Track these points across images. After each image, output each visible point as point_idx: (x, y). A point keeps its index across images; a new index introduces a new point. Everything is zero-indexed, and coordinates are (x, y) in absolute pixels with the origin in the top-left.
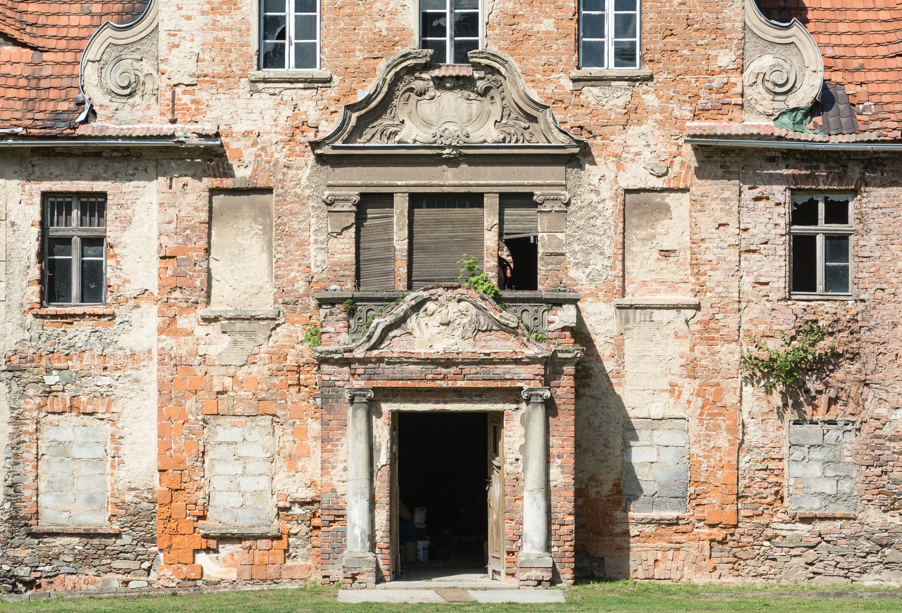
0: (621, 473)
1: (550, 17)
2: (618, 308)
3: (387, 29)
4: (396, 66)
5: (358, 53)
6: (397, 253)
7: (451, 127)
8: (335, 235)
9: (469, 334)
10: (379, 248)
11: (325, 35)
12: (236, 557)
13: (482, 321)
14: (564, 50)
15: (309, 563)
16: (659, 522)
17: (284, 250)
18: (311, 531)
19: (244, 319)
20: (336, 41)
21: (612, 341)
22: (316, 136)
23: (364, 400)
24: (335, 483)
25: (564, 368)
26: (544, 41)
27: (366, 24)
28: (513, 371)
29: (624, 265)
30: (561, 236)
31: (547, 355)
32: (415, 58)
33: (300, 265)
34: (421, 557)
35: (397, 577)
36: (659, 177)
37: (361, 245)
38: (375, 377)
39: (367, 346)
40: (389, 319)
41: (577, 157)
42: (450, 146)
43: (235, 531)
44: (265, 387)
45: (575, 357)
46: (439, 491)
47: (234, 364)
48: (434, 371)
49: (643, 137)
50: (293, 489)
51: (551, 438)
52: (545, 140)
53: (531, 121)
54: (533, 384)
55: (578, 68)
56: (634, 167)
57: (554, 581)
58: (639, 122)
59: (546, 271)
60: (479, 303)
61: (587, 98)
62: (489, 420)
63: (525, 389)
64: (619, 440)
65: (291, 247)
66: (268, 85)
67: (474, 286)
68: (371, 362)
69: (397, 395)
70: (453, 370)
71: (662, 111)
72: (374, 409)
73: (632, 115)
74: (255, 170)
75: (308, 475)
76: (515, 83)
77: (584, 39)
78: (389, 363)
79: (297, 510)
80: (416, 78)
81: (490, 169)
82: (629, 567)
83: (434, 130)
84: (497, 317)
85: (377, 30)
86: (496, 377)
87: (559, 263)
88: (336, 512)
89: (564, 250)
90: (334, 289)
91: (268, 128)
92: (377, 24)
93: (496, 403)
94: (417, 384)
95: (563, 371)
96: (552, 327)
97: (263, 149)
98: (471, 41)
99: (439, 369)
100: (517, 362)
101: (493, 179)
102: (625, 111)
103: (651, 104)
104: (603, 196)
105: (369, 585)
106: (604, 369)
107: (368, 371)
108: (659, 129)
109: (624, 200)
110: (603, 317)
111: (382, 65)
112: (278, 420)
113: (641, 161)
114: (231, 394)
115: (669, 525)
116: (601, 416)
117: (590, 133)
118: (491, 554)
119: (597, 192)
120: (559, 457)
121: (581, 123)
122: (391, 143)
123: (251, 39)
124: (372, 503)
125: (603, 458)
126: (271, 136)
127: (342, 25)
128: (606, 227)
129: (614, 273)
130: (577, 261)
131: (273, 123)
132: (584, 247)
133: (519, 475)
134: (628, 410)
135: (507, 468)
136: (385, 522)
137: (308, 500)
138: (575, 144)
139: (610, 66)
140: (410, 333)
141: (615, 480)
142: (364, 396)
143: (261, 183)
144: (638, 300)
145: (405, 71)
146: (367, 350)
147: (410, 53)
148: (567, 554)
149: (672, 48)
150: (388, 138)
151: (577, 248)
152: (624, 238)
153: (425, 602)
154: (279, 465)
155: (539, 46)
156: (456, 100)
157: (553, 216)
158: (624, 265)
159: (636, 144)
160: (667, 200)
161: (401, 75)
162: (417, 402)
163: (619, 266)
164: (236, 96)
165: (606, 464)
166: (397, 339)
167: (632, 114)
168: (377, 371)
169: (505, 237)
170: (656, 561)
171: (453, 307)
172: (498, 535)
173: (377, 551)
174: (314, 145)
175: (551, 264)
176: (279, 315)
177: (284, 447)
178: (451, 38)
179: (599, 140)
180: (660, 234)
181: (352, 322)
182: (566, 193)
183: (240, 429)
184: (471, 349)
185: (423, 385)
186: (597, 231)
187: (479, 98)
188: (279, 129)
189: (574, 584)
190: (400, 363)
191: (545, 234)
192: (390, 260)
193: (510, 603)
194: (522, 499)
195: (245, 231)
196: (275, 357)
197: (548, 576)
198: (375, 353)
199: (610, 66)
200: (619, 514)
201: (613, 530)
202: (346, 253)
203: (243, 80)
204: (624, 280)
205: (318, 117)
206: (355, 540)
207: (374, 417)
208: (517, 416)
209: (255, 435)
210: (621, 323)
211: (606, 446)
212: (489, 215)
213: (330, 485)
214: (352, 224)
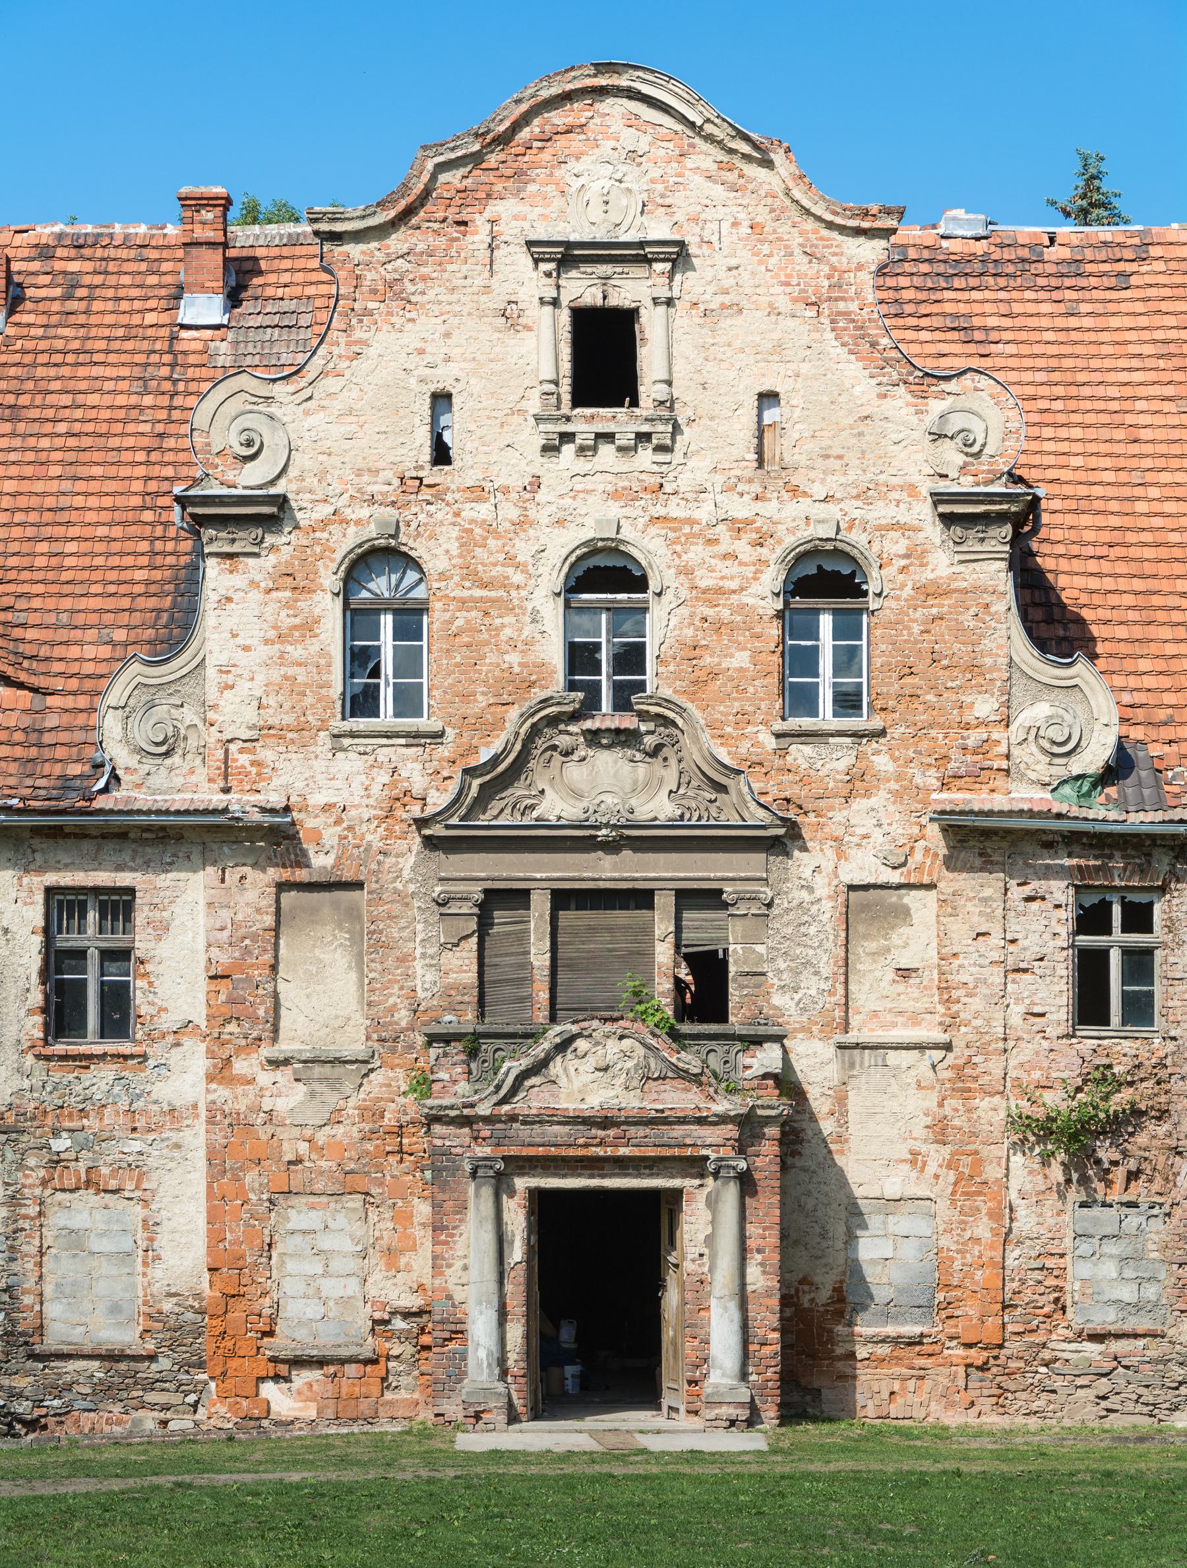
0: (844, 1273)
1: (745, 649)
3: (520, 664)
4: (532, 715)
5: (480, 698)
7: (609, 800)
9: (635, 1083)
10: (511, 965)
12: (315, 1387)
13: (653, 1066)
14: (764, 693)
15: (416, 1396)
16: (896, 1341)
17: (379, 967)
21: (831, 1092)
22: (423, 811)
23: (491, 1173)
24: (450, 1286)
25: (766, 1130)
27: (492, 658)
28: (695, 1134)
29: (847, 989)
30: (761, 949)
32: (559, 703)
33: (402, 988)
35: (536, 1416)
36: (894, 868)
38: (507, 1141)
39: (495, 1099)
40: (525, 1063)
41: (782, 840)
42: (607, 825)
43: (315, 1353)
45: (780, 1115)
53: (718, 791)
54: (722, 1152)
55: (783, 719)
56: (860, 854)
57: (752, 1421)
58: (867, 794)
62: (663, 1202)
64: (841, 1229)
65: (390, 962)
66: (357, 741)
67: (642, 1017)
68: (500, 1121)
70: (612, 1132)
71: (899, 778)
73: (858, 784)
74: (338, 858)
76: (696, 739)
78: (524, 1123)
79: (399, 1324)
81: (662, 857)
83: (585, 804)
84: (674, 1060)
86: (672, 1142)
87: (758, 986)
88: (453, 1327)
89: (765, 968)
91: (357, 801)
92: (507, 657)
93: (673, 1177)
94: (564, 1152)
97: (350, 828)
100: (701, 1121)
103: (883, 768)
104: (817, 894)
106: (820, 1132)
107: (497, 1133)
108: (894, 803)
111: (514, 713)
114: (307, 1164)
115: (909, 1344)
118: (665, 1384)
119: (811, 889)
120: (759, 1251)
121: (787, 794)
123: (333, 677)
125: (820, 1253)
127: (458, 659)
128: (822, 936)
134: (854, 1187)
135: (688, 1266)
136: (520, 1340)
139: (826, 715)
143: (348, 876)
144: (866, 1037)
154: (373, 1261)
155: (729, 689)
157: (749, 922)
158: (847, 989)
160: (906, 900)
162: (564, 1176)
163: (840, 990)
165: (824, 1261)
167: (857, 783)
169: (684, 950)
170: (892, 1393)
171: (613, 1046)
174: (421, 823)
178: (608, 677)
181: (473, 1066)
182: (767, 890)
184: (636, 1104)
185: (571, 1152)
187: (648, 759)
188: (371, 801)
189: (780, 1425)
193: (692, 1452)
194: (708, 1309)
196: (368, 1114)
197: (744, 1414)
198: (506, 1108)
199: (826, 715)
200: (840, 1329)
203: (322, 734)
208: (702, 1195)
209: (341, 1221)
211: (823, 1236)
212: (661, 920)
213: (445, 1289)
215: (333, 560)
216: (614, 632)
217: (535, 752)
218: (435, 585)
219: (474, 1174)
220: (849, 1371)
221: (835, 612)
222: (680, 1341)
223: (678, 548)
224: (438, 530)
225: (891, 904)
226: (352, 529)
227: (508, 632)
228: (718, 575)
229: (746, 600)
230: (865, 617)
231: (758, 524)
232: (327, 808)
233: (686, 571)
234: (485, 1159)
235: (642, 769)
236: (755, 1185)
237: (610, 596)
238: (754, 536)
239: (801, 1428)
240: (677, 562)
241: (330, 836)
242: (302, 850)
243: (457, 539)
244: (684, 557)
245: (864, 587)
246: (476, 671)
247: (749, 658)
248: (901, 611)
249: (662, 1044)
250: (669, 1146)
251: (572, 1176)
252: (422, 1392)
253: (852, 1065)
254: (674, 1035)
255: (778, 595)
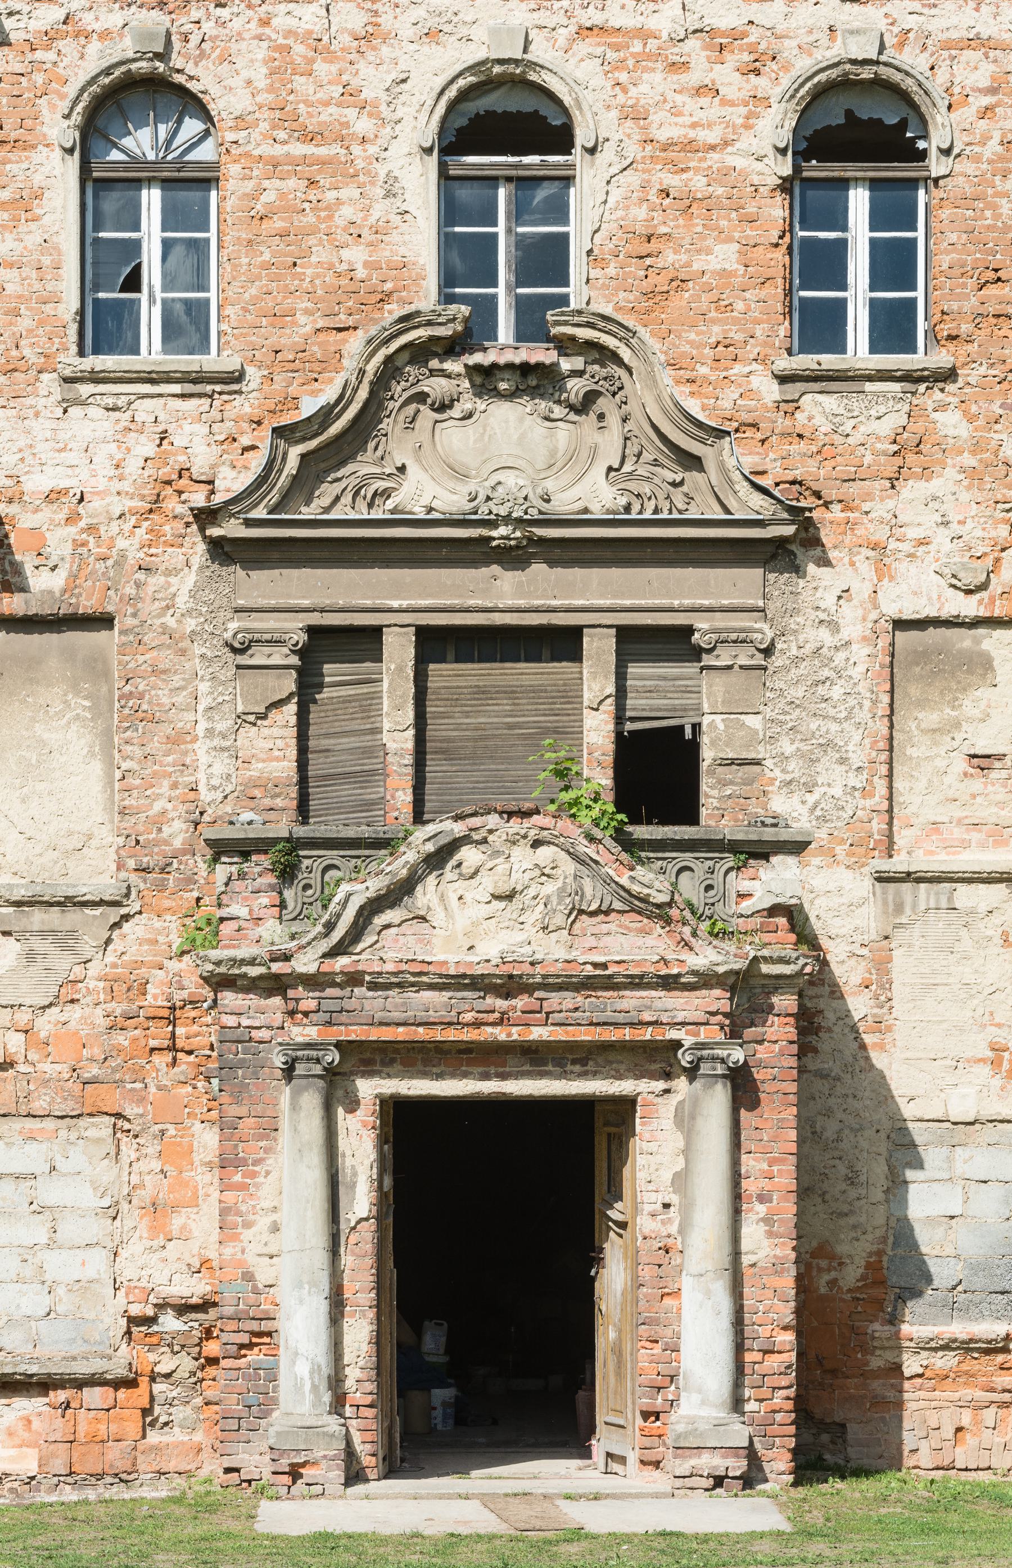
0: (884, 1240)
1: (730, 240)
2: (879, 880)
3: (366, 264)
4: (387, 341)
5: (302, 319)
6: (390, 758)
7: (511, 480)
8: (251, 718)
9: (559, 920)
10: (350, 750)
11: (228, 277)
12: (36, 1424)
13: (588, 891)
14: (762, 318)
15: (198, 1437)
16: (966, 1347)
17: (138, 752)
18: (202, 1368)
19: (51, 904)
20: (253, 291)
21: (864, 951)
22: (208, 499)
23: (318, 1070)
24: (251, 1258)
25: (775, 1000)
26: (714, 295)
27: (321, 254)
28: (658, 1004)
29: (890, 787)
30: (753, 722)
31: (736, 967)
32: (429, 323)
33: (174, 786)
34: (439, 1421)
35: (392, 1470)
36: (969, 592)
37: (312, 743)
38: (344, 1017)
39: (324, 946)
40: (375, 886)
41: (787, 546)
42: (507, 519)
43: (33, 1369)
44: (98, 1053)
45: (800, 973)
46: (488, 1276)
47: (28, 1002)
48: (480, 1005)
49: (935, 505)
50: (160, 1277)
51: (744, 1157)
52: (717, 508)
53: (687, 468)
54: (704, 1034)
55: (790, 353)
56: (913, 569)
57: (751, 1478)
58: (926, 472)
59: (720, 799)
60: (581, 849)
61: (810, 418)
62: (599, 1123)
63: (687, 1044)
64: (880, 1169)
65: (155, 745)
66: (102, 388)
67: (570, 810)
68: (334, 984)
69: (392, 1061)
70: (520, 1002)
71: (977, 448)
72: (340, 1093)
73: (911, 458)
74: (73, 577)
75: (194, 1246)
76: (653, 381)
77: (803, 294)
78: (374, 986)
79: (170, 1322)
80: (432, 373)
81: (596, 574)
82: (901, 1443)
83: (472, 486)
84: (624, 881)
85: (344, 266)
86: (621, 1018)
87: (749, 782)
88: (254, 1326)
89: (760, 752)
90: (249, 822)
91: (102, 484)
92: (345, 254)
93: (620, 1077)
94: (439, 1035)
95: (772, 1007)
96: (747, 906)
97: (91, 529)
98: (553, 295)
99: (491, 1001)
100: (669, 983)
101: (602, 596)
102: (895, 448)
103: (951, 432)
104: (845, 634)
105: (330, 1489)
106: (848, 1014)
107: (326, 1005)
108: (969, 488)
109: (893, 644)
110: (844, 900)
111: (355, 344)
112: (127, 1126)
113: (930, 558)
114: (22, 1068)
115: (987, 1352)
116: (840, 1115)
117: (818, 495)
118: (601, 1417)
119: (834, 626)
120: (762, 1199)
121: (797, 474)
122: (377, 514)
123: (62, 286)
124: (337, 1304)
125: (845, 1208)
126: (108, 500)
127: (267, 256)
128: (852, 702)
129: (869, 803)
130: (788, 777)
131: (112, 472)
132: (805, 747)
133: (670, 1242)
134: (902, 1102)
135: (644, 1224)
136: (365, 1347)
137: (195, 1300)
138: (785, 515)
139: (858, 349)
140: (424, 919)
141: (870, 1254)
142: (318, 1061)
143: (87, 605)
144: (920, 863)
145: (406, 356)
146: (324, 956)
147: (418, 313)
148: (779, 1417)
149: (999, 309)
150: (370, 505)
151: (787, 747)
152: (891, 727)
153: (464, 1531)
154: (129, 1223)
155: (704, 306)
156: (521, 420)
157: (736, 677)
158: (890, 787)
159: (919, 521)
160: (986, 645)
161: (399, 363)
162: (439, 1076)
163: (881, 787)
164: (31, 413)
165: (852, 1220)
166: (393, 931)
167: (909, 455)
168: (347, 1004)
169: (629, 726)
170: (959, 1429)
171: (523, 857)
172: (619, 1374)
173: (349, 1411)
174: (206, 516)
175: (732, 783)
176: (127, 895)
177: (142, 1186)
178: (509, 288)
179: (836, 512)
180: (970, 720)
181: (288, 894)
182: (765, 627)
183: (44, 1146)
184: (562, 954)
185: (452, 1035)
186: (832, 712)
187: (573, 417)
188: (126, 486)
189: (795, 1484)
190: (399, 985)
191: (718, 718)
192: (374, 776)
193: (663, 1534)
194: (677, 1293)
195: (52, 711)
196: (120, 988)
197: (738, 1466)
198: (342, 962)
199: (858, 349)
200: (878, 1328)
201: (867, 1364)
202: (277, 759)
203: (45, 377)
204: (891, 818)
205: (213, 460)
206: (298, 1388)
207: (340, 1111)
208: (667, 1107)
209: (77, 1159)
210: (885, 913)
211: (851, 1180)
212: (594, 675)
213: (241, 1264)
214: (291, 694)
215: (62, 97)
216: (519, 213)
217: (391, 405)
218: (230, 136)
219: (289, 1072)
220: (891, 1395)
221: (875, 184)
222: (628, 1347)
223: (623, 77)
224: (234, 47)
225: (960, 652)
226: (94, 46)
227: (347, 212)
228: (688, 120)
229: (732, 161)
230: (921, 193)
231: (752, 39)
232: (53, 496)
233: (635, 115)
234: (308, 1046)
235: (563, 433)
236: (756, 1090)
237: (517, 159)
238: (746, 57)
239: (824, 1487)
240: (621, 99)
241: (60, 542)
242: (13, 564)
243: (265, 62)
244: (633, 92)
245: (921, 145)
246: (294, 276)
247: (738, 254)
248: (982, 179)
249: (607, 855)
250: (615, 1024)
251: (453, 1076)
252: (207, 1432)
253: (899, 908)
254: (622, 839)
255: (783, 151)
